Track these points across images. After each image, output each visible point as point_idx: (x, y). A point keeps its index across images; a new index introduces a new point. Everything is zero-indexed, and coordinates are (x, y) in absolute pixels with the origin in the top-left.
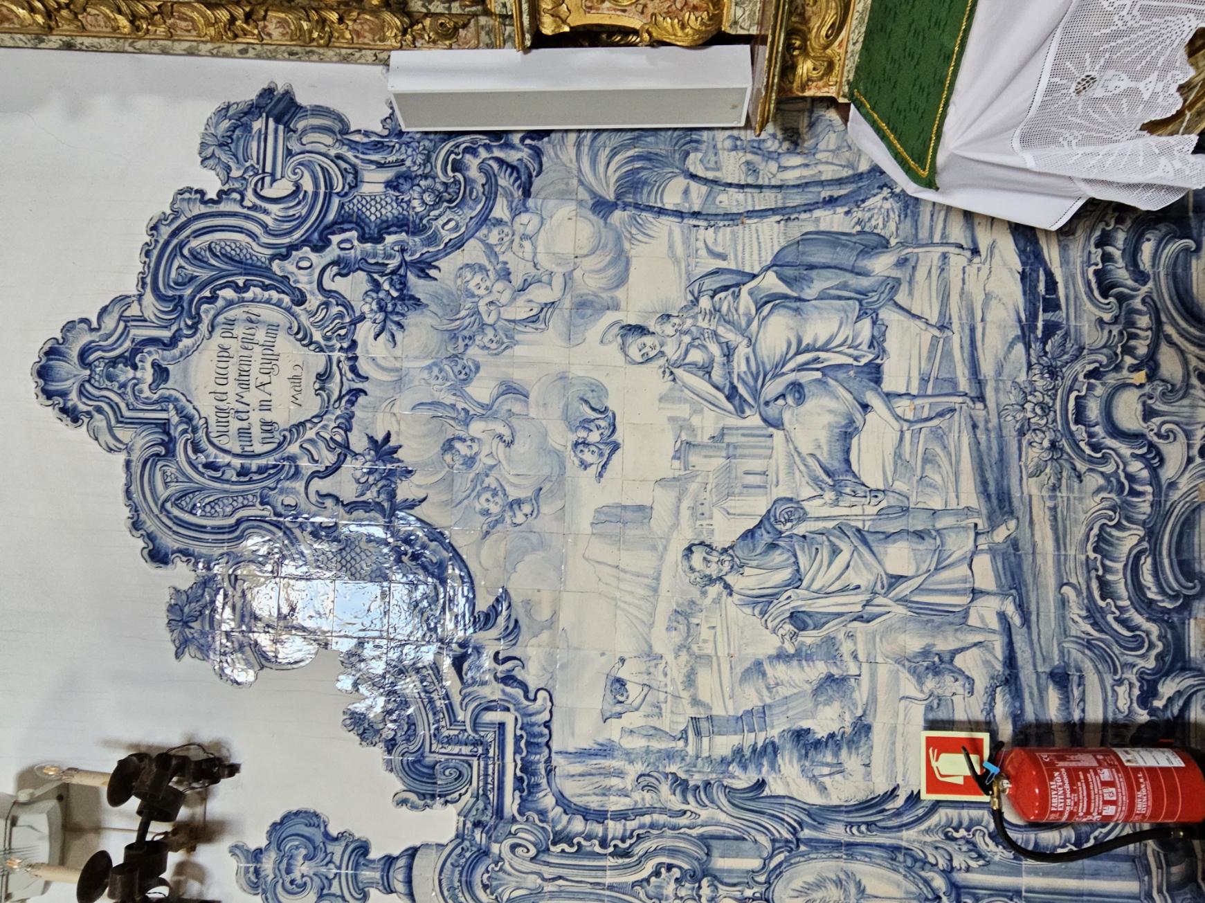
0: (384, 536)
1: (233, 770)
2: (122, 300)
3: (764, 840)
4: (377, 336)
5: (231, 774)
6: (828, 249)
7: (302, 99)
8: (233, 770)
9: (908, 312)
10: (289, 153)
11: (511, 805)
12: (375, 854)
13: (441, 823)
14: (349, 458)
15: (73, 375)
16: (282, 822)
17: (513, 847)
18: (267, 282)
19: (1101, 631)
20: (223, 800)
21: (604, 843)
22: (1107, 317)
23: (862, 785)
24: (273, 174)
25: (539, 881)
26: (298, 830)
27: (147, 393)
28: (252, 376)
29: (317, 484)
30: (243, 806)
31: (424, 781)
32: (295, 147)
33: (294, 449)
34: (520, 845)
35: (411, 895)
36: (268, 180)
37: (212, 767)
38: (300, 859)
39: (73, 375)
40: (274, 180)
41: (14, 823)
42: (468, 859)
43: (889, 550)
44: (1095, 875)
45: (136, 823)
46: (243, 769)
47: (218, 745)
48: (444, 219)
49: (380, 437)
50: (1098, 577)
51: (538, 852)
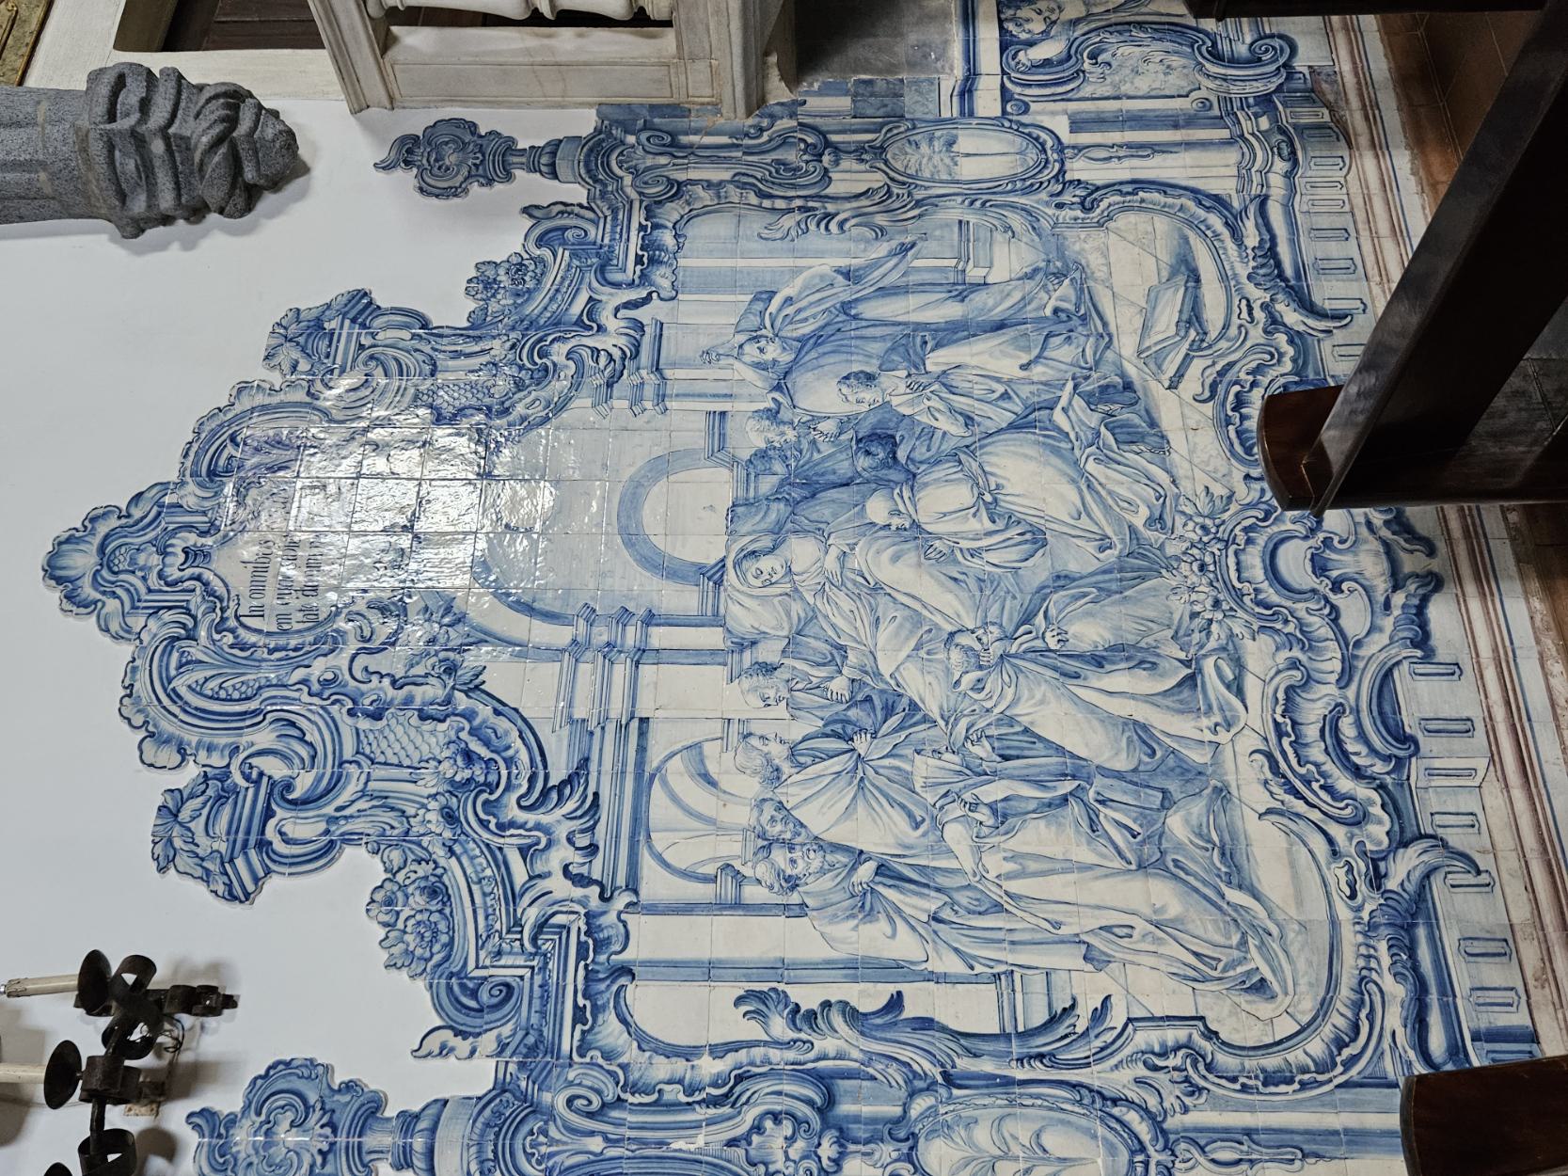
0: (613, 715)
1: (230, 1002)
2: (164, 486)
3: (895, 1074)
6: (1444, 1045)
7: (382, 300)
8: (230, 1002)
10: (362, 347)
12: (391, 1112)
13: (473, 1074)
15: (106, 563)
16: (266, 1076)
20: (212, 1039)
21: (690, 1091)
22: (1256, 472)
26: (287, 1086)
30: (233, 1046)
32: (366, 341)
34: (579, 1097)
35: (431, 1170)
37: (208, 1000)
38: (286, 1125)
39: (106, 563)
42: (506, 1114)
43: (421, 984)
50: (1322, 787)
51: (604, 1105)
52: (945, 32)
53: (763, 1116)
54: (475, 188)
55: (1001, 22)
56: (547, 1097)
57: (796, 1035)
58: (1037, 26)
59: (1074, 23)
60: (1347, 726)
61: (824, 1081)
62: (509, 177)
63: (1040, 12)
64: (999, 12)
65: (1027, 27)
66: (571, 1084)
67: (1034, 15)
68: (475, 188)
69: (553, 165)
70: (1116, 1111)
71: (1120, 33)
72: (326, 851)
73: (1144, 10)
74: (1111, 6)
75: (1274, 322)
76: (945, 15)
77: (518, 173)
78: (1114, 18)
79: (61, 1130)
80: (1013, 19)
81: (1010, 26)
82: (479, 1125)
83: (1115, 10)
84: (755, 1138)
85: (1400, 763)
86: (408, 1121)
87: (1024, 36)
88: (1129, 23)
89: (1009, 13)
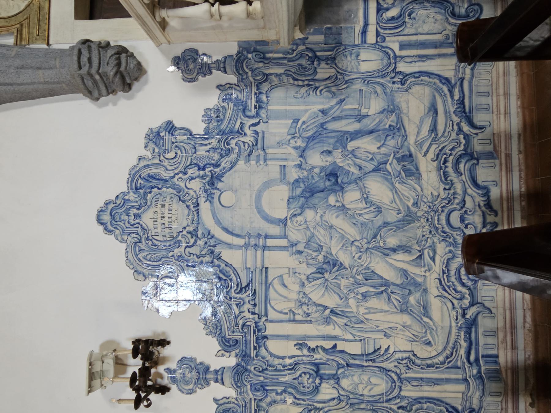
1: (168, 343)
4: (205, 202)
5: (168, 391)
8: (168, 343)
9: (400, 351)
11: (253, 354)
12: (212, 369)
14: (198, 240)
17: (255, 369)
18: (168, 186)
19: (385, 51)
20: (165, 351)
21: (284, 367)
23: (334, 155)
24: (168, 150)
27: (133, 222)
28: (164, 216)
29: (188, 249)
30: (172, 353)
31: (227, 345)
33: (180, 238)
36: (167, 152)
40: (168, 152)
41: (103, 362)
44: (428, 373)
45: (141, 362)
46: (172, 342)
47: (164, 333)
48: (225, 161)
49: (208, 203)
56: (249, 367)
66: (254, 364)
75: (460, 130)
86: (216, 372)
87: (385, 6)
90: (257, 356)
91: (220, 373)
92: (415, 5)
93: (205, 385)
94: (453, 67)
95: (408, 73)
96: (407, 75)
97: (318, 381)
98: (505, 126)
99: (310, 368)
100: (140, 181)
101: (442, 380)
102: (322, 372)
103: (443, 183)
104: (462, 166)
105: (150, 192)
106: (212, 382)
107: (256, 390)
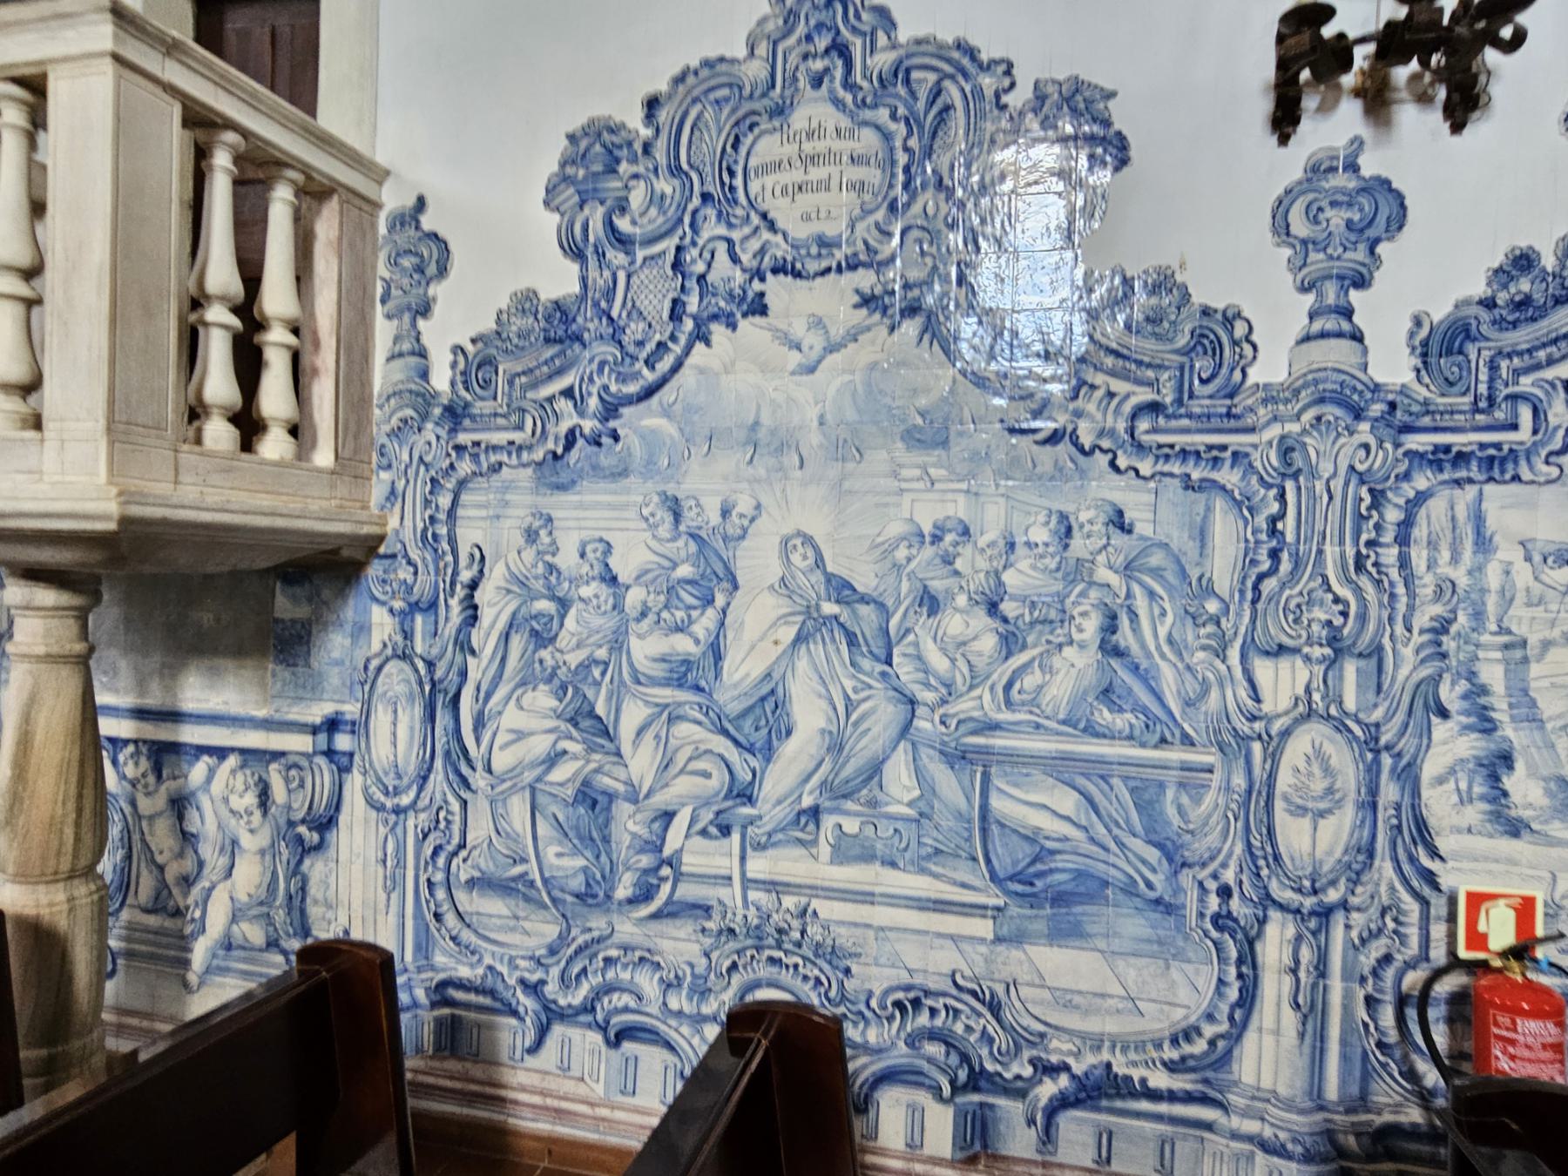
16: (1391, 190)
20: (1419, 123)
21: (1370, 544)
25: (1326, 475)
29: (722, 248)
52: (126, 693)
53: (1347, 604)
54: (1288, 252)
55: (136, 742)
56: (429, 426)
57: (1416, 631)
58: (130, 771)
59: (133, 803)
60: (627, 999)
61: (433, 605)
62: (1304, 289)
63: (144, 775)
64: (145, 742)
65: (131, 763)
66: (1380, 446)
67: (142, 769)
68: (437, 290)
69: (401, 355)
70: (415, 787)
71: (122, 839)
72: (575, 251)
73: (143, 865)
74: (148, 838)
75: (1052, 1070)
76: (142, 694)
77: (396, 322)
78: (136, 837)
79: (449, 114)
80: (137, 753)
81: (131, 748)
82: (1310, 377)
83: (143, 840)
84: (1330, 596)
85: (603, 1028)
86: (1347, 313)
87: (121, 758)
88: (130, 848)
89: (144, 749)
90: (459, 449)
91: (1346, 326)
92: (120, 827)
93: (1300, 277)
94: (1266, 1083)
95: (1258, 947)
96: (1251, 943)
97: (398, 605)
98: (513, 1089)
99: (423, 586)
100: (932, 77)
101: (1322, 1036)
102: (419, 619)
103: (887, 993)
104: (934, 1049)
105: (894, 116)
106: (1309, 299)
107: (1286, 452)
